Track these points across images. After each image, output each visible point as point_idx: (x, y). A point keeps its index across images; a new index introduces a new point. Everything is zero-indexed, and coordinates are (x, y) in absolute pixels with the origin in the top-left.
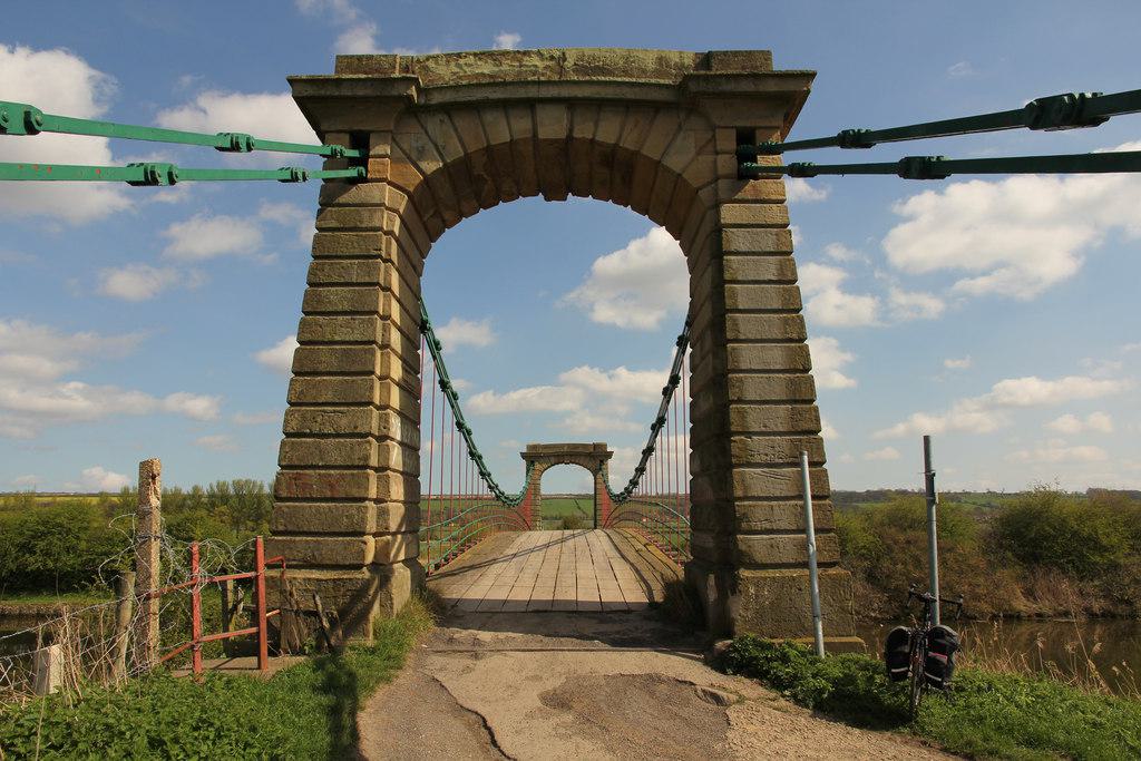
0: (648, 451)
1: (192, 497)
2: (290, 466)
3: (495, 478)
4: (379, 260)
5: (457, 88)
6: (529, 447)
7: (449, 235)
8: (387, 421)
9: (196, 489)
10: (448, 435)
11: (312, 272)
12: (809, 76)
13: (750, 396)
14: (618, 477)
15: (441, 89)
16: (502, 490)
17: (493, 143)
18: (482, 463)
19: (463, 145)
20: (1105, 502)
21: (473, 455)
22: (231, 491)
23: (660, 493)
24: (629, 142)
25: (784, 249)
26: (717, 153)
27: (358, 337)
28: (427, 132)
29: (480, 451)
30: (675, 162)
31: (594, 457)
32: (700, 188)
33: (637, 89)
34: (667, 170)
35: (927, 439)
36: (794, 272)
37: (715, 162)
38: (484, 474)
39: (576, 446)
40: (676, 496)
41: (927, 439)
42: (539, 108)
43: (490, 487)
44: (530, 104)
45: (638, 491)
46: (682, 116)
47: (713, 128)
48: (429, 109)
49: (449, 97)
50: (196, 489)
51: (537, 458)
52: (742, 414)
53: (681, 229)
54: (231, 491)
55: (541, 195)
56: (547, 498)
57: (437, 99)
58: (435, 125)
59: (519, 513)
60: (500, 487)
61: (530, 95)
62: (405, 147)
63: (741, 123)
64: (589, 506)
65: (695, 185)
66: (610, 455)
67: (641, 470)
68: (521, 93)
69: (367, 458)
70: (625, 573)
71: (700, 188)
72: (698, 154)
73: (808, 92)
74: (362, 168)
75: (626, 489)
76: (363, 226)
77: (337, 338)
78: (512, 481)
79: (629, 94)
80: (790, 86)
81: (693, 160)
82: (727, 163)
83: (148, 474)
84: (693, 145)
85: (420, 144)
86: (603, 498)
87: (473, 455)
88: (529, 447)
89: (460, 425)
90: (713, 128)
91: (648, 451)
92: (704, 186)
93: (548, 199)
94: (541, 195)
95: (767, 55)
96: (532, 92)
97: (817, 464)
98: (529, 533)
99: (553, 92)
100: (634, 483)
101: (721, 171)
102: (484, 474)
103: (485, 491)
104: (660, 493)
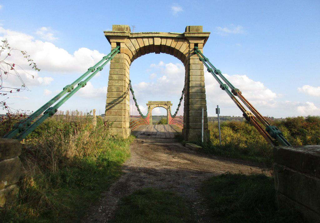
1: (66, 116)
4: (123, 70)
9: (68, 112)
11: (110, 71)
17: (145, 45)
19: (139, 46)
20: (310, 120)
22: (70, 114)
24: (173, 46)
25: (202, 69)
27: (120, 85)
29: (136, 98)
31: (167, 104)
33: (174, 35)
36: (204, 74)
39: (214, 77)
42: (155, 38)
43: (140, 113)
45: (177, 115)
49: (136, 36)
50: (68, 112)
53: (184, 61)
54: (70, 114)
57: (134, 36)
69: (122, 108)
77: (116, 85)
86: (169, 117)
89: (134, 98)
96: (154, 35)
97: (205, 110)
100: (176, 113)
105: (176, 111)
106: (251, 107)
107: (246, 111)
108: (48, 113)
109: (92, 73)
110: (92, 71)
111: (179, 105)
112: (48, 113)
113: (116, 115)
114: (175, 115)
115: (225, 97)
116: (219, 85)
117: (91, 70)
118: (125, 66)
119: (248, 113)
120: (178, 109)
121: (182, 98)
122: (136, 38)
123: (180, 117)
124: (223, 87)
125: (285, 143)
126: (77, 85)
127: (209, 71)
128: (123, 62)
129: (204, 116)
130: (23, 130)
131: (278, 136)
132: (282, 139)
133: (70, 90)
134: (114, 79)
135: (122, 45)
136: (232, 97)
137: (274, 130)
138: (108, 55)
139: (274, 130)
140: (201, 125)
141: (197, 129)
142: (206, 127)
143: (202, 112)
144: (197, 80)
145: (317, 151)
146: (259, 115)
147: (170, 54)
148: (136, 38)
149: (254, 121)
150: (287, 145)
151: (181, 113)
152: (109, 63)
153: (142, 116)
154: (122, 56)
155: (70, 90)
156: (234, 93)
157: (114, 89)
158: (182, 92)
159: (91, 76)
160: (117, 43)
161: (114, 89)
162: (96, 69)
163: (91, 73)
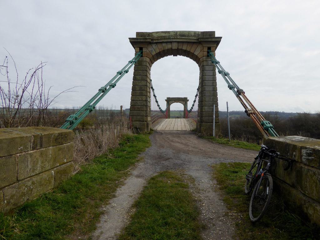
2: (184, 109)
3: (160, 106)
5: (158, 40)
6: (138, 34)
8: (147, 98)
10: (152, 97)
12: (221, 38)
13: (206, 95)
15: (155, 40)
24: (188, 50)
29: (158, 100)
31: (184, 101)
35: (227, 102)
37: (203, 53)
38: (158, 106)
41: (227, 102)
43: (159, 108)
44: (171, 42)
45: (193, 110)
46: (198, 44)
47: (203, 47)
48: (153, 43)
49: (157, 41)
51: (169, 101)
52: (205, 98)
56: (172, 111)
58: (154, 46)
59: (167, 114)
61: (171, 41)
63: (208, 46)
64: (183, 114)
65: (200, 58)
66: (188, 100)
68: (169, 40)
73: (220, 41)
78: (164, 107)
79: (188, 41)
80: (217, 40)
82: (206, 53)
83: (121, 107)
88: (138, 34)
90: (203, 47)
95: (214, 32)
96: (171, 40)
99: (175, 40)
100: (192, 108)
102: (158, 106)
105: (192, 106)
106: (251, 105)
107: (247, 108)
108: (89, 110)
109: (120, 75)
110: (120, 74)
111: (195, 101)
112: (89, 110)
113: (139, 111)
114: (191, 110)
115: (231, 94)
116: (227, 85)
117: (120, 73)
118: (147, 68)
119: (249, 110)
120: (193, 105)
121: (197, 95)
122: (156, 43)
123: (195, 112)
124: (231, 88)
125: (274, 134)
126: (109, 87)
127: (220, 72)
128: (145, 64)
129: (215, 112)
130: (73, 123)
131: (270, 129)
132: (272, 132)
133: (104, 91)
134: (137, 79)
135: (144, 50)
136: (238, 96)
137: (267, 124)
138: (133, 59)
139: (267, 124)
140: (213, 119)
141: (209, 122)
142: (217, 121)
143: (213, 108)
144: (209, 80)
145: (292, 140)
146: (256, 112)
147: (187, 57)
148: (156, 43)
149: (253, 116)
150: (276, 136)
151: (196, 108)
152: (134, 66)
153: (161, 110)
154: (145, 59)
155: (104, 91)
156: (240, 93)
157: (138, 88)
158: (197, 90)
159: (120, 77)
160: (140, 47)
161: (138, 88)
162: (123, 72)
163: (120, 76)
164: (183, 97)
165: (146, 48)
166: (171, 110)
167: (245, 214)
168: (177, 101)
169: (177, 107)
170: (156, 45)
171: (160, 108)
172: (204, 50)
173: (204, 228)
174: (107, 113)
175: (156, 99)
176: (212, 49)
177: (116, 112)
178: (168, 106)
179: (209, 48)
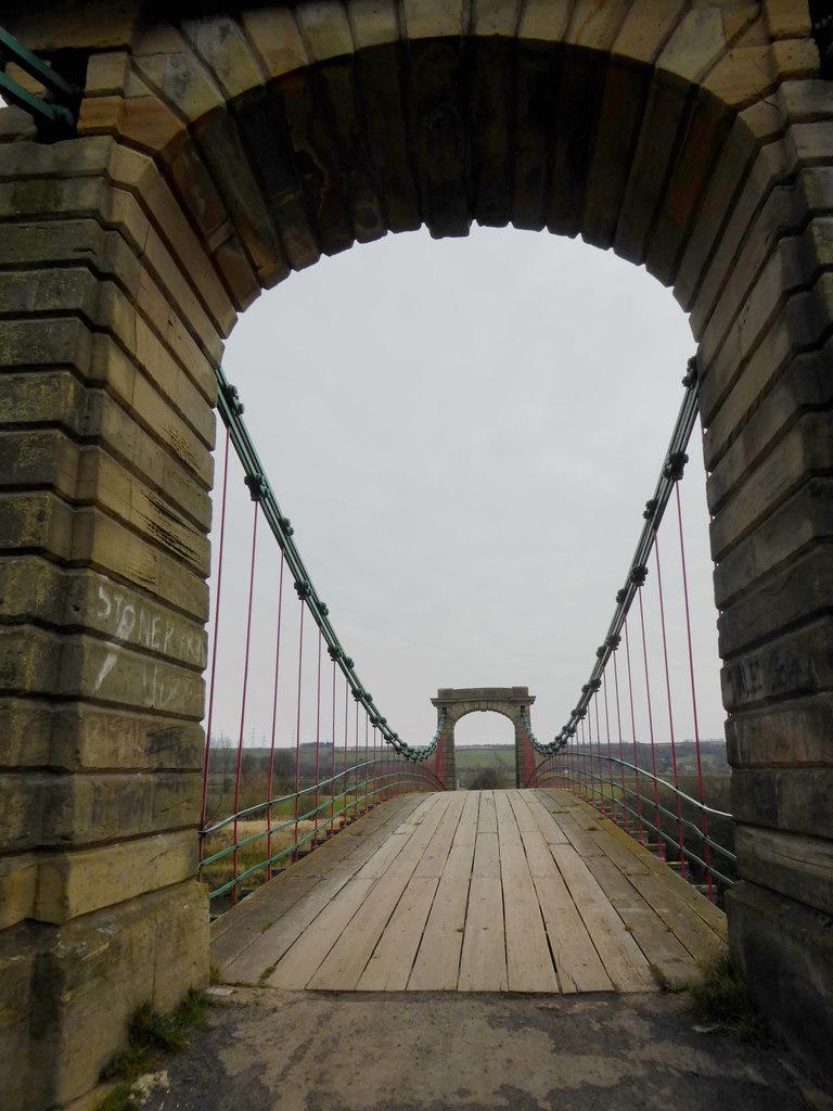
0: (593, 686)
2: (517, 739)
3: (393, 725)
7: (269, 301)
14: (545, 729)
16: (560, 730)
18: (372, 706)
21: (360, 695)
23: (581, 743)
26: (772, 39)
28: (196, 53)
29: (368, 690)
30: (684, 62)
31: (515, 702)
32: (742, 106)
34: (670, 81)
38: (377, 721)
40: (698, 748)
43: (386, 737)
51: (451, 704)
55: (424, 228)
60: (400, 737)
62: (153, 76)
64: (510, 759)
66: (531, 700)
67: (579, 713)
70: (90, 89)
71: (742, 106)
72: (730, 45)
74: (65, 111)
75: (557, 739)
76: (62, 208)
78: (420, 731)
81: (719, 59)
84: (719, 29)
85: (182, 69)
87: (360, 695)
89: (335, 653)
91: (593, 686)
92: (750, 102)
93: (437, 233)
94: (424, 228)
98: (438, 795)
100: (569, 730)
101: (786, 66)
102: (377, 721)
103: (380, 742)
104: (581, 743)
105: (566, 719)
114: (560, 741)
153: (401, 749)
164: (509, 685)
165: (123, 56)
166: (456, 744)
167: (513, 776)
168: (483, 705)
169: (484, 731)
170: (233, 26)
171: (391, 737)
172: (777, 23)
173: (557, 1050)
174: (227, 762)
175: (352, 679)
176: (526, 708)
177: (258, 756)
178: (444, 727)
179: (523, 707)
